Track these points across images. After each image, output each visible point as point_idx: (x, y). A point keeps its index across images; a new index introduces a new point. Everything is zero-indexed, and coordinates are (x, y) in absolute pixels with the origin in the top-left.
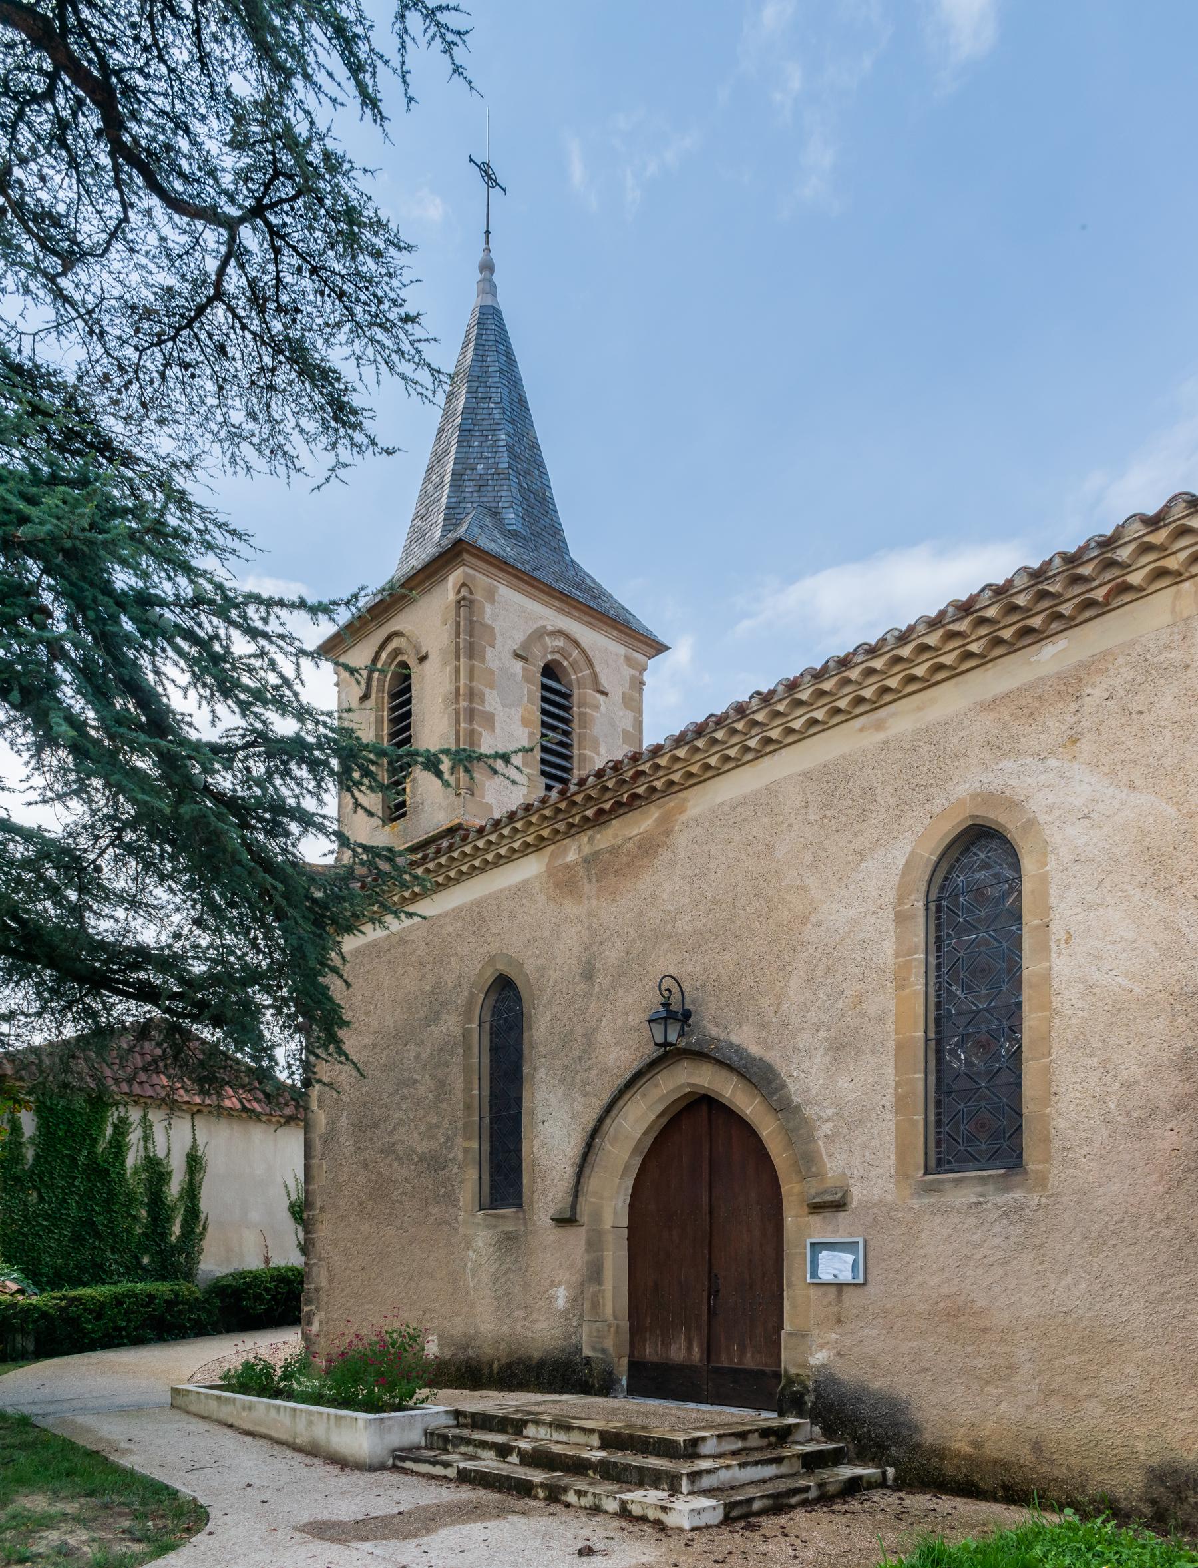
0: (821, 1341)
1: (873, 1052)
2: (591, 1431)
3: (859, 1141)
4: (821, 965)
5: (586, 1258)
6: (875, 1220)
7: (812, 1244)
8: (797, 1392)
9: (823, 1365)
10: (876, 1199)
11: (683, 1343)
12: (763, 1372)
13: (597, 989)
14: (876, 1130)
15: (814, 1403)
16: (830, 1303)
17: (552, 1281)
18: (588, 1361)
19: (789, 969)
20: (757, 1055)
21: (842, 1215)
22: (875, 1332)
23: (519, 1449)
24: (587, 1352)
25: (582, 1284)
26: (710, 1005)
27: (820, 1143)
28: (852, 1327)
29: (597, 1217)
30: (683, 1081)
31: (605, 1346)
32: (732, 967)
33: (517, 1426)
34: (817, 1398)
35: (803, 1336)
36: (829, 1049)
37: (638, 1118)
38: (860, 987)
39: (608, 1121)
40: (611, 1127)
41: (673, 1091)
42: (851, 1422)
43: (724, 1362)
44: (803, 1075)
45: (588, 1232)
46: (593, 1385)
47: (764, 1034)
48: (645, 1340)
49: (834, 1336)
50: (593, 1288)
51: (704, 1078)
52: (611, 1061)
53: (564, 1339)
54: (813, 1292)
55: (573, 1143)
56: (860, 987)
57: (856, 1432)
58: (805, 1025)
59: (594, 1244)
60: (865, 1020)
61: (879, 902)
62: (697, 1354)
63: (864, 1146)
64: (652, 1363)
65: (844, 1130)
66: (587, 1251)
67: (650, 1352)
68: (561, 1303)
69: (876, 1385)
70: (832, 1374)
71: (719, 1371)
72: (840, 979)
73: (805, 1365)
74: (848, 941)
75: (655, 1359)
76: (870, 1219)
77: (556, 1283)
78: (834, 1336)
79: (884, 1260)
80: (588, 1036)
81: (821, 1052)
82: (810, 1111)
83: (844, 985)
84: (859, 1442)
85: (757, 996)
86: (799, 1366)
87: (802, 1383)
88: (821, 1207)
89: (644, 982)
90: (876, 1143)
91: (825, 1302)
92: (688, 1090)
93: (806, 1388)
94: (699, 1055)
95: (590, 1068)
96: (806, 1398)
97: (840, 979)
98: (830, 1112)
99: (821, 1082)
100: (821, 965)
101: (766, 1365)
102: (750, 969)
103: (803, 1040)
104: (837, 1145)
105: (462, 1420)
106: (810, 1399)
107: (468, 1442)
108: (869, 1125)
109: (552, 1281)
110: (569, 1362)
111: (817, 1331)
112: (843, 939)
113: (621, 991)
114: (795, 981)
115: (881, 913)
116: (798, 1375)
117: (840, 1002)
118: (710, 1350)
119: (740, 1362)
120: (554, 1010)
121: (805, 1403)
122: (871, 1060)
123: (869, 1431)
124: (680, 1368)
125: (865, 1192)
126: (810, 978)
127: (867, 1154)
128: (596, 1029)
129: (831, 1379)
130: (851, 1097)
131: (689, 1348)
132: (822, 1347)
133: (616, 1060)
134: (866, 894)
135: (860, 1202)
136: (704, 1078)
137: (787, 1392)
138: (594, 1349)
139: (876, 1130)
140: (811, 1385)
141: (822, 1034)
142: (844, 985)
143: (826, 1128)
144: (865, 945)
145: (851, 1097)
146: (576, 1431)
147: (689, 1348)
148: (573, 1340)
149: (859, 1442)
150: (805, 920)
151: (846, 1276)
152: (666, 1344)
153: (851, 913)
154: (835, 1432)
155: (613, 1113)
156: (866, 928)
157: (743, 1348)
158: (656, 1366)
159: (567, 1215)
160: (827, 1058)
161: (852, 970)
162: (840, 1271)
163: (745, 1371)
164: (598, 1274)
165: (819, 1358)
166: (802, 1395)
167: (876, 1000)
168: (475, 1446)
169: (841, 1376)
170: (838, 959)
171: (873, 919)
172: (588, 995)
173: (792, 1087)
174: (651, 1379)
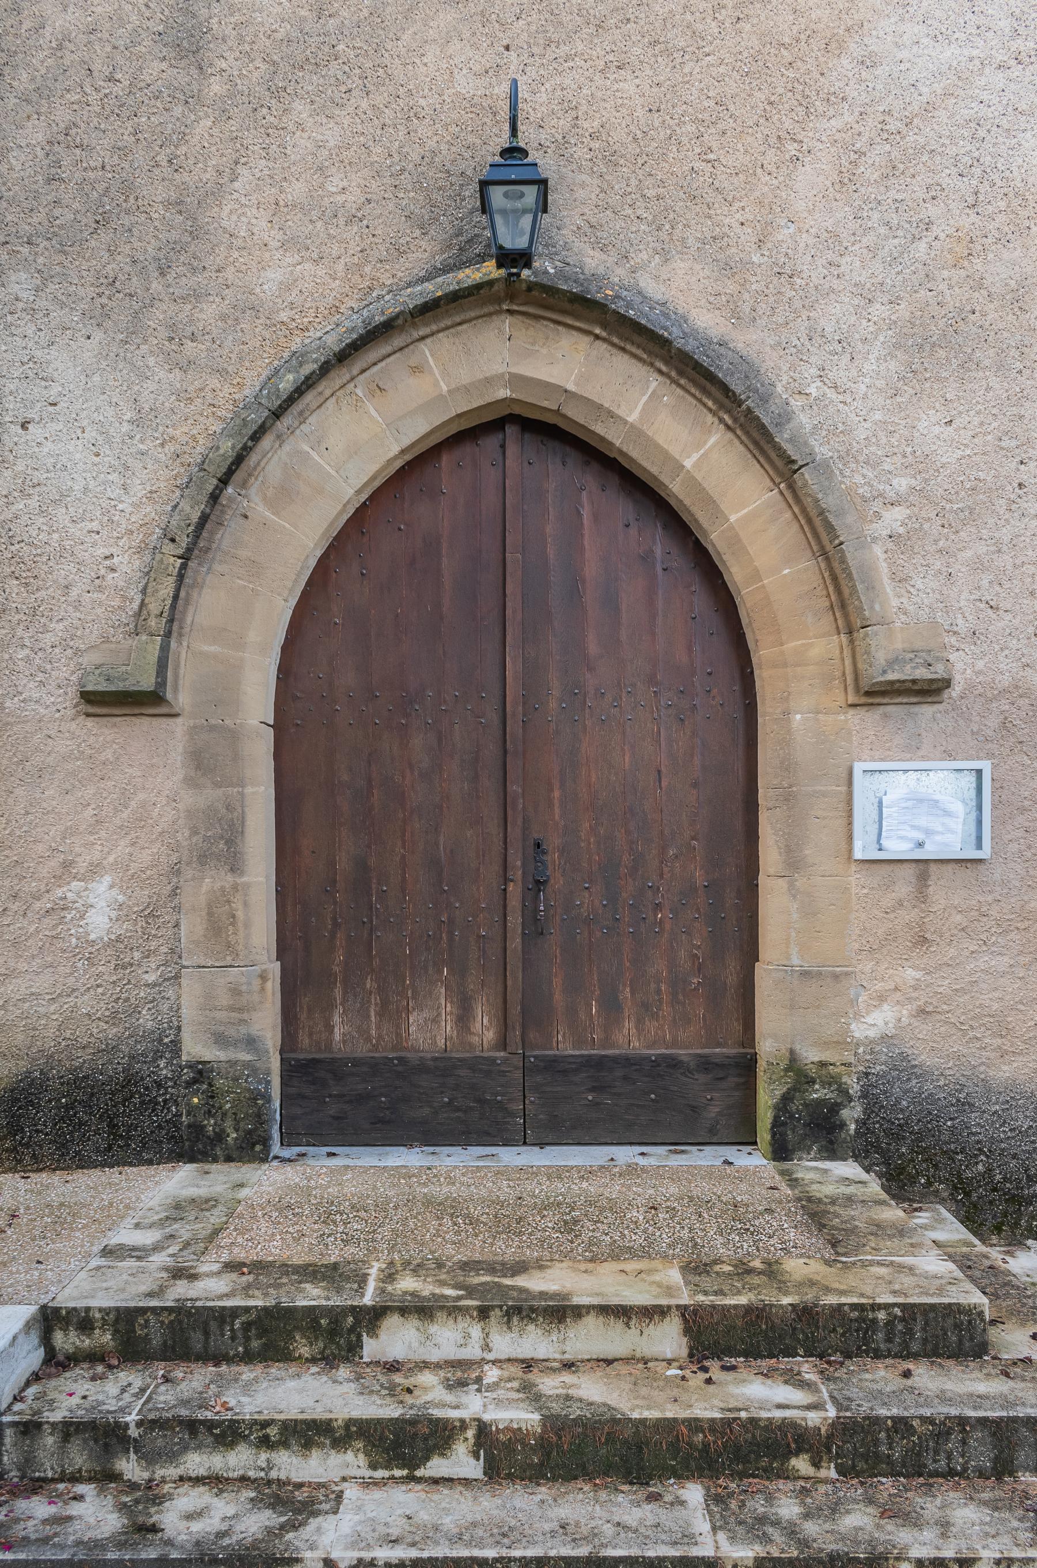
0: (879, 986)
1: (1000, 367)
2: (653, 1313)
3: (969, 554)
4: (877, 155)
5: (188, 799)
6: (1005, 724)
7: (979, 772)
8: (820, 1103)
9: (884, 1038)
10: (1006, 681)
11: (447, 1008)
12: (673, 1063)
13: (216, 87)
14: (1005, 534)
15: (861, 1123)
16: (900, 903)
17: (67, 865)
18: (202, 1073)
19: (792, 148)
20: (715, 333)
21: (927, 711)
22: (1002, 962)
23: (483, 1428)
24: (195, 1047)
25: (176, 871)
26: (580, 194)
27: (878, 550)
28: (952, 952)
29: (222, 692)
30: (501, 369)
31: (255, 1030)
32: (640, 113)
33: (333, 1333)
34: (868, 1111)
35: (836, 977)
36: (897, 346)
37: (353, 443)
38: (968, 220)
39: (266, 442)
40: (273, 460)
41: (466, 390)
42: (950, 1155)
43: (563, 1045)
44: (831, 394)
45: (193, 731)
46: (220, 1137)
47: (731, 287)
48: (331, 1006)
49: (911, 974)
50: (214, 880)
51: (566, 367)
52: (270, 288)
53: (113, 1018)
54: (855, 879)
55: (139, 491)
56: (968, 220)
57: (959, 1176)
58: (836, 283)
59: (208, 761)
60: (980, 296)
61: (1014, 45)
62: (484, 1030)
63: (979, 566)
64: (357, 1062)
65: (933, 528)
66: (190, 782)
67: (342, 1032)
68: (99, 922)
69: (1003, 1072)
70: (904, 1057)
71: (554, 1066)
72: (921, 194)
73: (842, 1042)
74: (942, 115)
75: (362, 1050)
76: (993, 722)
77: (82, 866)
78: (911, 974)
79: (1023, 810)
80: (191, 210)
81: (877, 349)
82: (857, 478)
83: (932, 211)
84: (967, 1194)
85: (710, 196)
86: (826, 1045)
87: (833, 1081)
88: (883, 693)
89: (379, 100)
90: (1005, 560)
91: (888, 901)
92: (504, 393)
93: (843, 1091)
94: (579, 307)
95: (197, 296)
96: (845, 1113)
97: (921, 194)
98: (902, 483)
99: (878, 416)
100: (877, 155)
101: (675, 1044)
102: (690, 128)
103: (835, 314)
104: (918, 560)
105: (65, 1341)
106: (851, 1114)
107: (228, 1433)
108: (991, 521)
109: (67, 865)
110: (130, 1081)
111: (869, 966)
112: (929, 108)
113: (300, 109)
114: (811, 178)
115: (1016, 71)
116: (823, 1064)
117: (922, 246)
118: (521, 1015)
119: (607, 1042)
120: (63, 116)
121: (843, 1125)
122: (994, 382)
123: (989, 1170)
124: (443, 1067)
125: (980, 665)
126: (846, 180)
127: (985, 583)
128: (216, 193)
129: (904, 1067)
130: (949, 457)
131: (464, 1019)
132: (882, 998)
133: (286, 287)
134: (981, 20)
135: (970, 687)
136: (566, 367)
137: (795, 1106)
138: (221, 1040)
139: (1005, 534)
140: (855, 1088)
141: (879, 310)
142: (932, 211)
143: (894, 518)
144: (982, 133)
145: (949, 457)
146: (591, 1321)
147: (464, 1019)
148: (146, 1020)
149: (967, 1194)
150: (833, 45)
151: (950, 838)
152: (393, 1013)
153: (949, 53)
154: (913, 1180)
155: (287, 420)
156: (985, 96)
157: (612, 1007)
158: (374, 1067)
159: (147, 682)
160: (893, 365)
161: (947, 178)
162: (928, 832)
163: (627, 1061)
164: (230, 842)
165: (874, 1022)
166: (835, 1108)
167: (1006, 255)
168: (265, 1443)
169: (925, 1058)
170: (920, 150)
171: (999, 79)
172: (192, 99)
173: (804, 420)
174: (340, 1099)
